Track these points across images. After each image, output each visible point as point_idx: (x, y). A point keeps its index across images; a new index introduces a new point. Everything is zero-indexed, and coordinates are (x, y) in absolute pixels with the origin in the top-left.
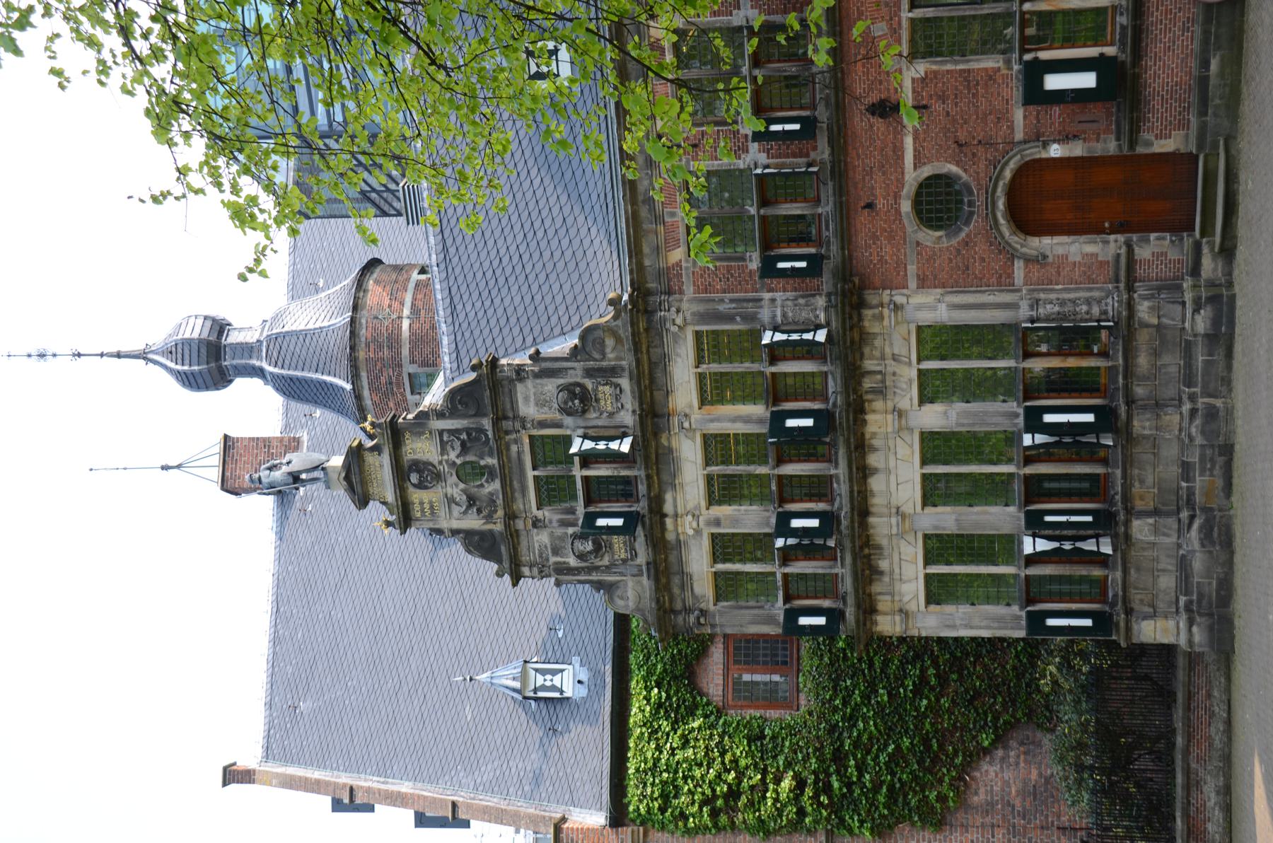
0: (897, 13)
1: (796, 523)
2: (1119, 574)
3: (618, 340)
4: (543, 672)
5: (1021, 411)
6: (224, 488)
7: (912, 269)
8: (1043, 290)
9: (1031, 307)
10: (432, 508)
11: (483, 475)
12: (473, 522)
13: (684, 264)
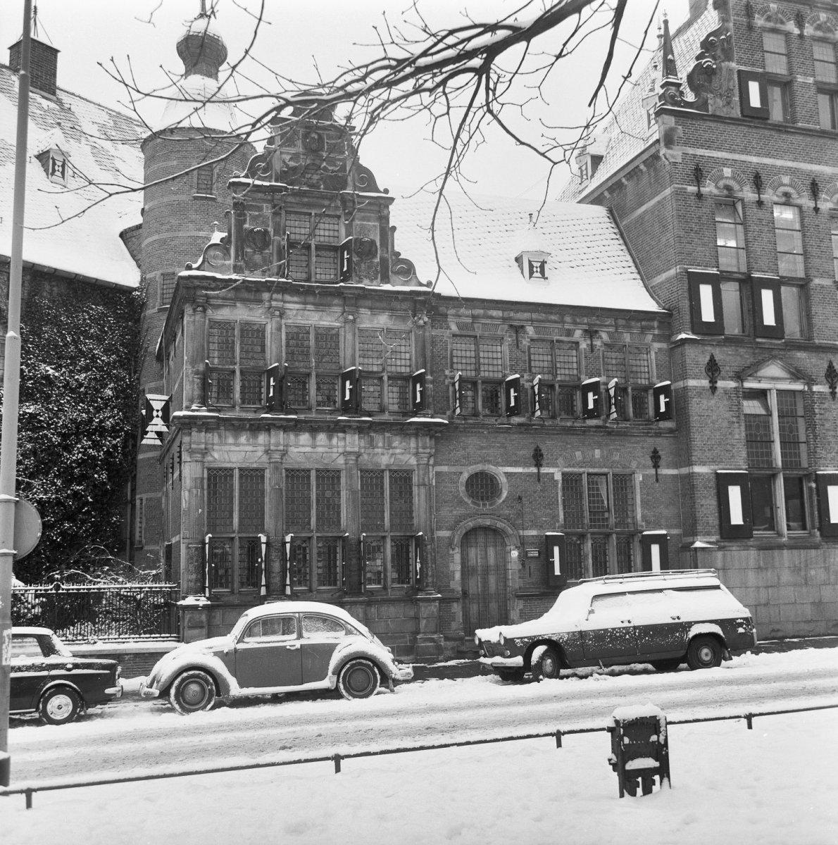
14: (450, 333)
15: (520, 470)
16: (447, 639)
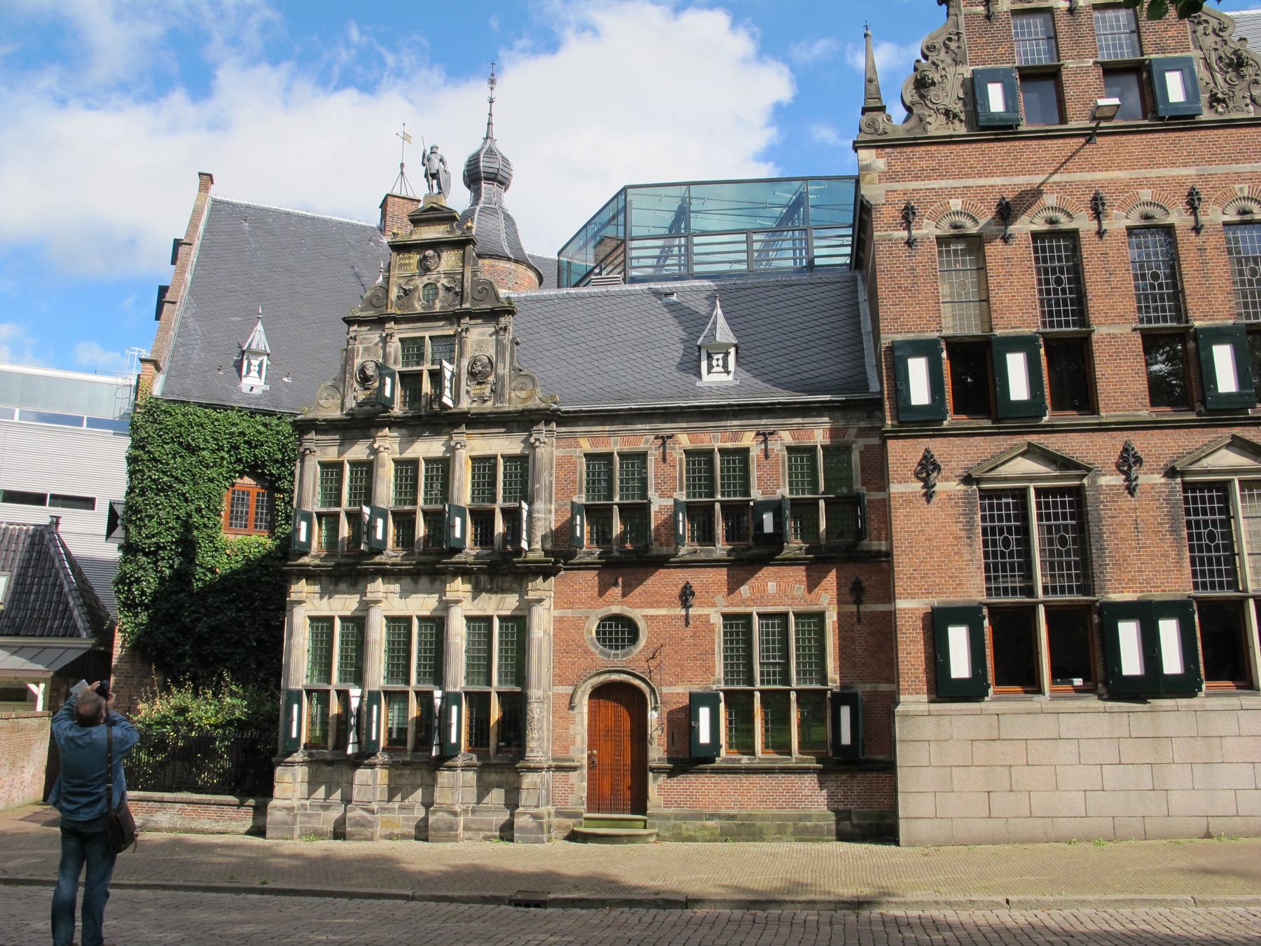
0: (755, 604)
1: (380, 522)
2: (329, 757)
3: (525, 400)
4: (260, 365)
5: (458, 690)
6: (388, 195)
7: (569, 613)
8: (549, 707)
9: (539, 698)
10: (405, 265)
11: (428, 301)
12: (394, 293)
13: (578, 450)
14: (580, 452)
15: (663, 612)
16: (559, 814)
